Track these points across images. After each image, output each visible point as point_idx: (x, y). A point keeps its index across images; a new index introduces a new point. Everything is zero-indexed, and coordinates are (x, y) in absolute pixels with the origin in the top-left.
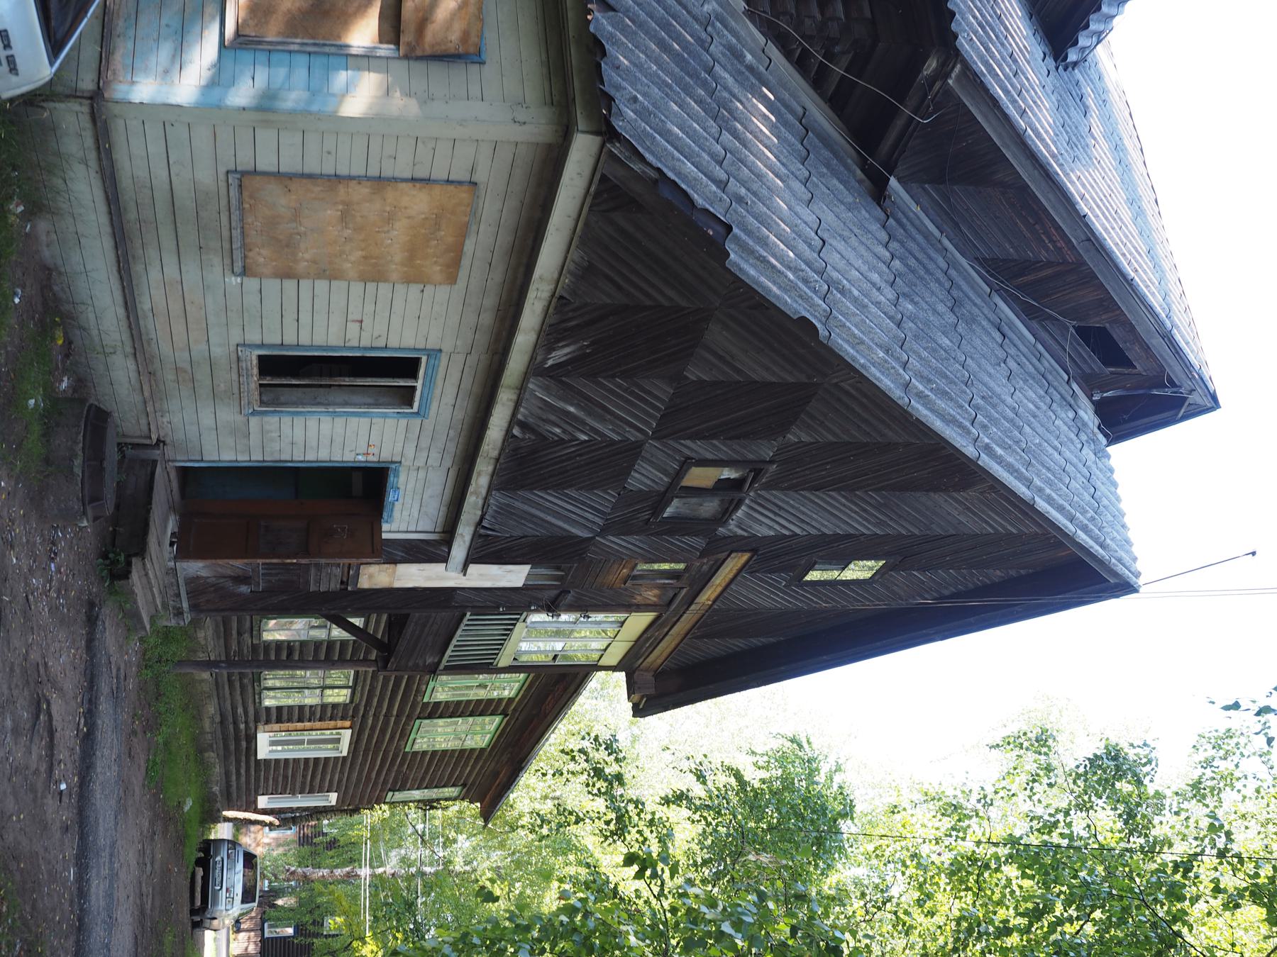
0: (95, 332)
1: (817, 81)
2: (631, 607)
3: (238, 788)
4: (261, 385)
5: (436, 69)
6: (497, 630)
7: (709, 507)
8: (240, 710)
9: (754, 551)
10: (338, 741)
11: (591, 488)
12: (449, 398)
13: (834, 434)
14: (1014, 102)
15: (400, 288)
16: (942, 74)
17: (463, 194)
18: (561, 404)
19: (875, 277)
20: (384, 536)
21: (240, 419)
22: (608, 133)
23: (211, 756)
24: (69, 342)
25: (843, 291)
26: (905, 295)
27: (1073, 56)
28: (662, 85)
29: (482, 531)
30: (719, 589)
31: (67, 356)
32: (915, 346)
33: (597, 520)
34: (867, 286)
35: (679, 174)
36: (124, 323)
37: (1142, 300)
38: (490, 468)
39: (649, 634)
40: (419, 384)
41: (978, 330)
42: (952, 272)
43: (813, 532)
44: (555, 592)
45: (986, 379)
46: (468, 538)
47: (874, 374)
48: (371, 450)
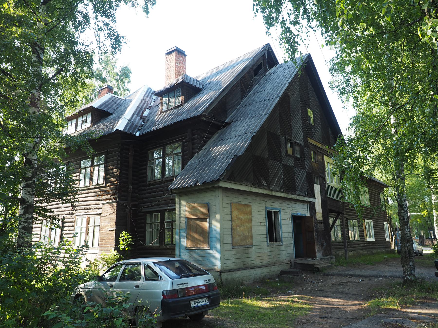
0: (266, 274)
1: (209, 138)
2: (323, 161)
3: (384, 245)
4: (276, 241)
5: (210, 211)
6: (331, 189)
7: (297, 148)
8: (361, 245)
9: (307, 137)
10: (368, 223)
12: (276, 204)
13: (278, 125)
14: (209, 101)
15: (253, 215)
16: (205, 116)
17: (233, 205)
18: (275, 182)
19: (244, 123)
20: (309, 215)
21: (283, 246)
22: (219, 180)
23: (374, 251)
24: (269, 279)
25: (247, 130)
26: (248, 116)
27: (201, 87)
28: (210, 170)
29: (306, 195)
30: (317, 143)
31: (272, 279)
32: (257, 113)
33: (302, 171)
34: (246, 125)
35: (226, 166)
36: (264, 268)
37: (246, 66)
38: (290, 195)
40: (273, 210)
41: (255, 98)
42: (244, 105)
43: (301, 125)
44: (321, 178)
45: (264, 96)
46: (307, 198)
47: (262, 122)
48: (289, 219)
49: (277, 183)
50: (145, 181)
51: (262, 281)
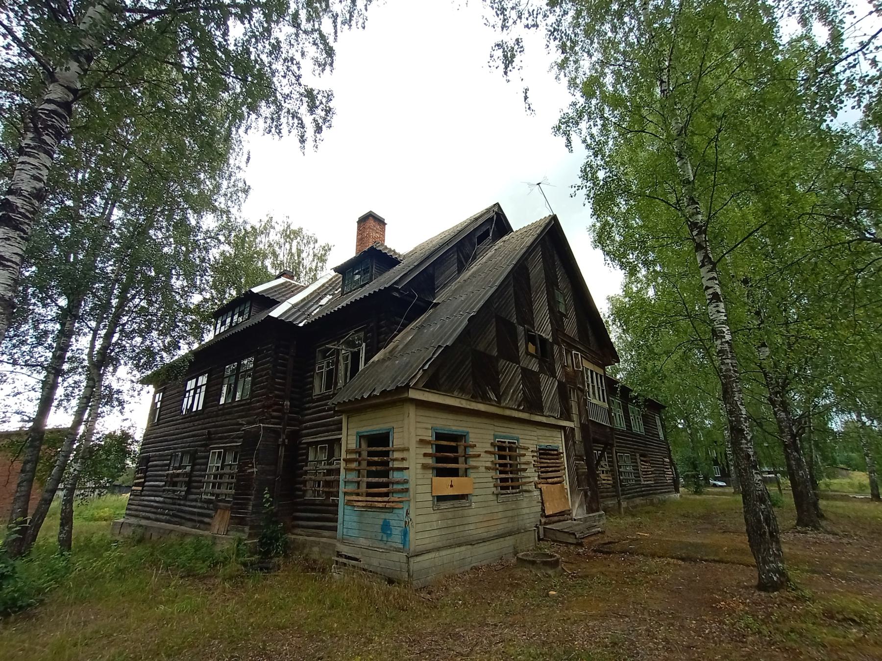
1: (404, 326)
11: (540, 383)
12: (511, 431)
16: (397, 290)
22: (407, 387)
39: (565, 303)
49: (512, 396)
50: (311, 395)
51: (526, 259)
